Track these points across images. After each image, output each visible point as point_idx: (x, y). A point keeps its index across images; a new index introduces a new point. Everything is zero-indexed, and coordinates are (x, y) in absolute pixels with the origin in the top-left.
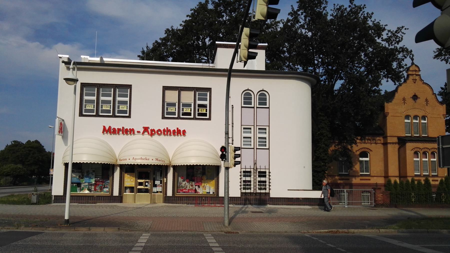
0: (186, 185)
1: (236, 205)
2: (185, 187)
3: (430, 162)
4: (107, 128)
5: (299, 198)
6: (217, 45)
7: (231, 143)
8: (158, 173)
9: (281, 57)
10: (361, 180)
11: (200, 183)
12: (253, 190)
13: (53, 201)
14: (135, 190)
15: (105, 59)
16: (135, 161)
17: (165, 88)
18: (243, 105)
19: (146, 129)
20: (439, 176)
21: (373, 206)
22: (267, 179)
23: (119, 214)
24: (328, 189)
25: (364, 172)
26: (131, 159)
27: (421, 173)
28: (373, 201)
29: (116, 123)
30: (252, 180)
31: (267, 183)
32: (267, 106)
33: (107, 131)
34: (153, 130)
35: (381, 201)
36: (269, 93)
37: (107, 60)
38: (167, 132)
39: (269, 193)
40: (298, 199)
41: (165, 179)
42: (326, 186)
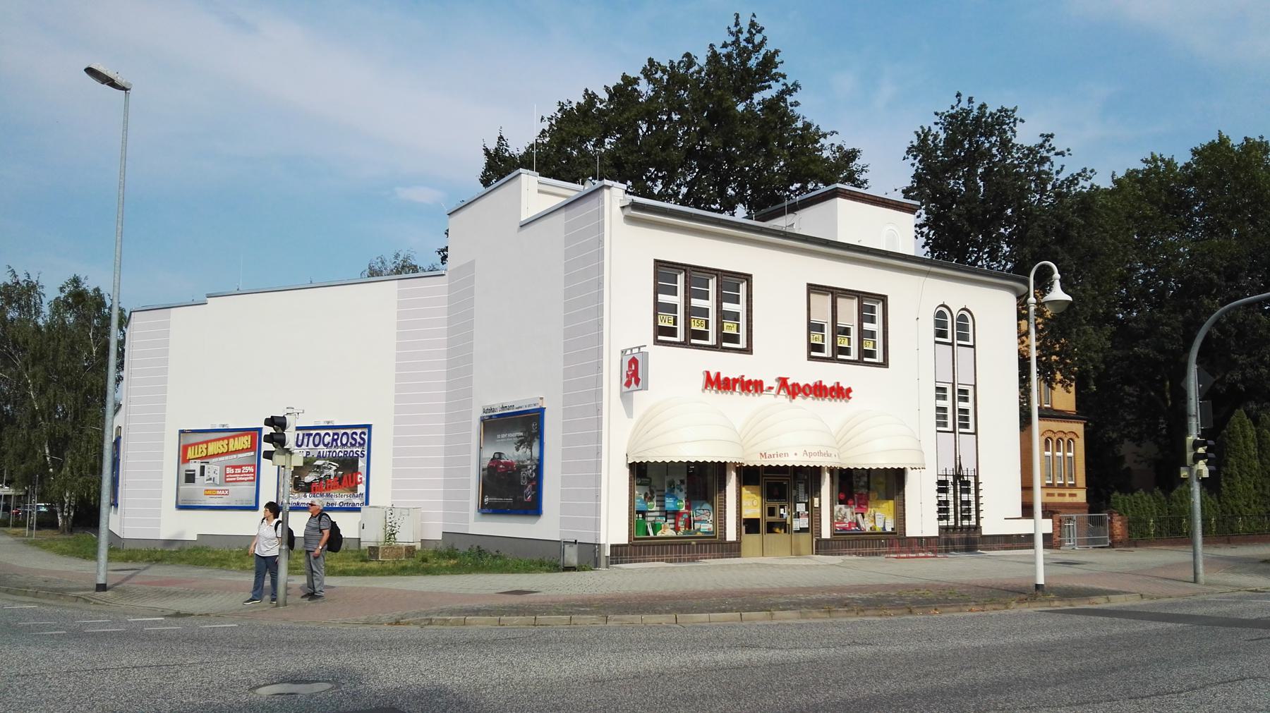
0: (843, 513)
2: (839, 518)
3: (1066, 459)
4: (713, 376)
6: (839, 192)
8: (800, 485)
11: (865, 507)
12: (953, 520)
13: (603, 562)
14: (763, 526)
16: (810, 459)
17: (813, 289)
19: (783, 382)
20: (1078, 486)
21: (1108, 545)
22: (972, 497)
24: (322, 527)
26: (800, 453)
27: (1053, 481)
28: (1108, 537)
29: (729, 365)
30: (951, 499)
31: (973, 506)
32: (971, 343)
33: (717, 383)
34: (795, 385)
35: (1119, 535)
36: (974, 316)
38: (819, 390)
39: (977, 527)
41: (816, 500)
42: (320, 519)
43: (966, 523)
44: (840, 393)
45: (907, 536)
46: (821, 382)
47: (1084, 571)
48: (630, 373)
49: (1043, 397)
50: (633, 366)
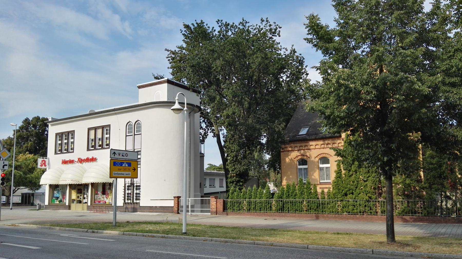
4: (63, 161)
18: (127, 134)
22: (127, 192)
23: (315, 236)
29: (67, 157)
33: (65, 162)
38: (88, 160)
43: (129, 201)
44: (93, 160)
47: (261, 238)
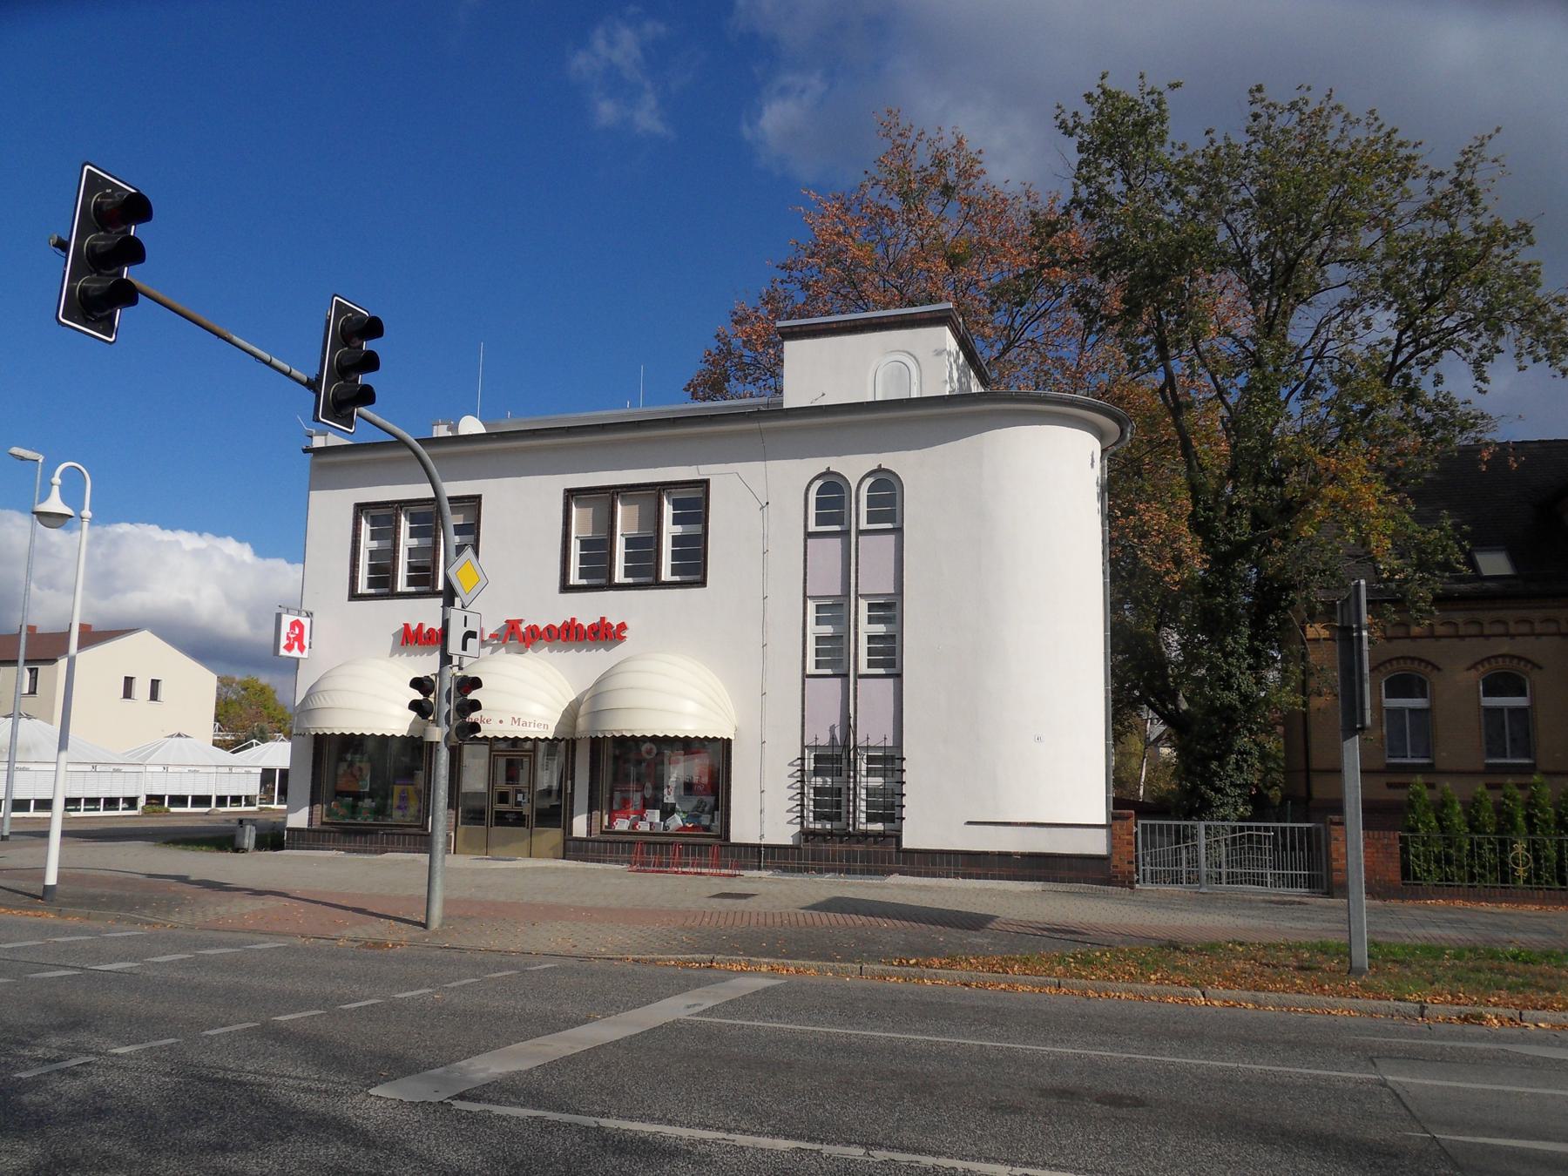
1: (784, 871)
5: (1007, 855)
7: (14, 735)
9: (779, 338)
10: (1390, 786)
14: (489, 816)
15: (274, 359)
25: (1505, 756)
34: (533, 630)
37: (275, 361)
40: (1005, 856)
45: (732, 840)
46: (573, 620)
48: (292, 636)
49: (1324, 858)
50: (297, 631)
